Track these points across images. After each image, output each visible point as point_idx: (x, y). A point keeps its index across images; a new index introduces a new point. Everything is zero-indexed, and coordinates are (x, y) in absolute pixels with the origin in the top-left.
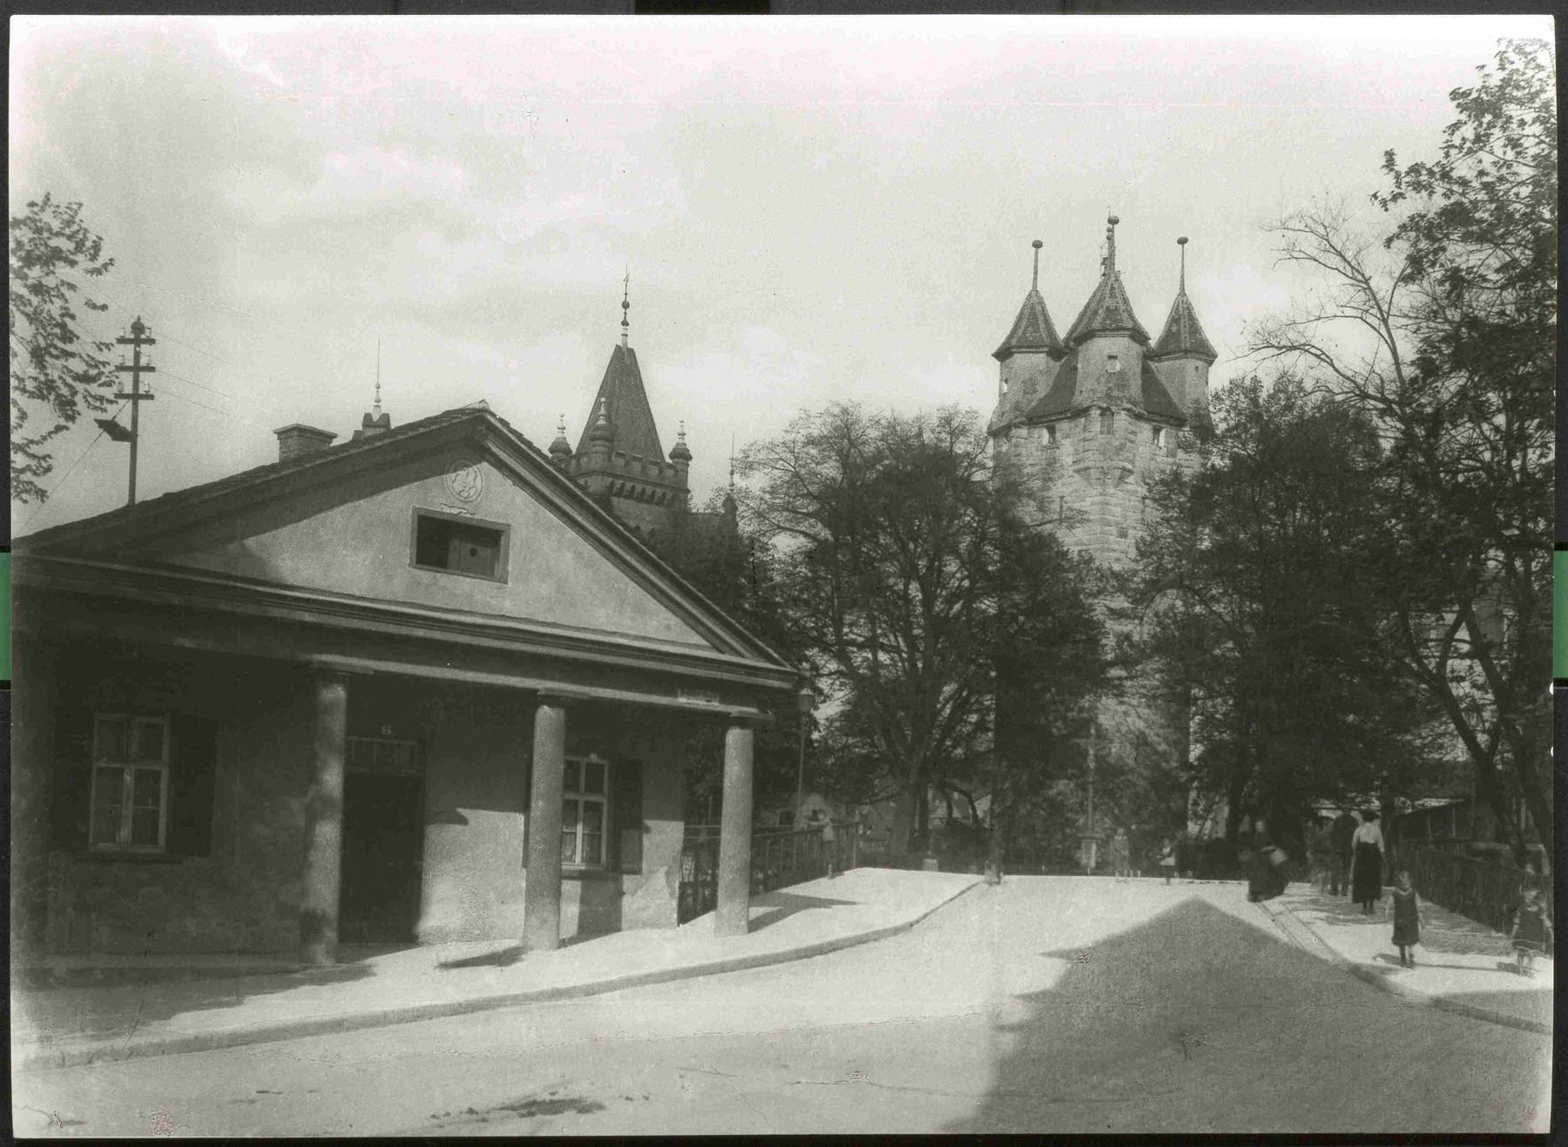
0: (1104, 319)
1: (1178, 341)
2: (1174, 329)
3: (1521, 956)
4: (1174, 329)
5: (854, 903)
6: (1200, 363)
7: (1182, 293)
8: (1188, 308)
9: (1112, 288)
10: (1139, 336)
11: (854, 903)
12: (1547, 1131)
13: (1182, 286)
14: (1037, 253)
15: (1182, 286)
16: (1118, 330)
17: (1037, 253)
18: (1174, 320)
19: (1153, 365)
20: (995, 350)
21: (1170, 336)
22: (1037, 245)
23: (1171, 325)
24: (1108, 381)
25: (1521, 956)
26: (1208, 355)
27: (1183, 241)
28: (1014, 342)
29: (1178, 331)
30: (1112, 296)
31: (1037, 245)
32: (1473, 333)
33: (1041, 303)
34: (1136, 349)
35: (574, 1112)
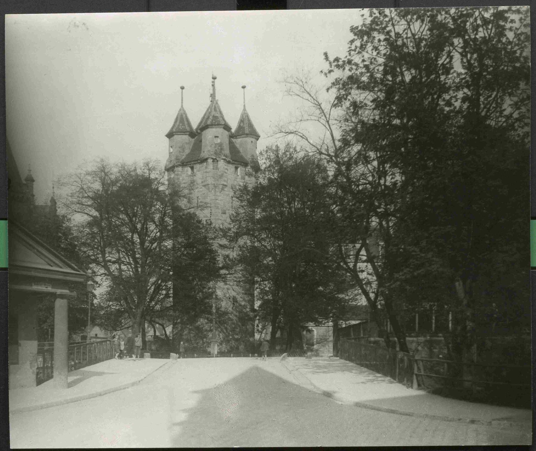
0: (212, 120)
2: (242, 124)
6: (253, 140)
8: (247, 116)
9: (215, 107)
10: (227, 128)
18: (242, 121)
22: (182, 88)
23: (240, 123)
27: (244, 87)
31: (182, 88)
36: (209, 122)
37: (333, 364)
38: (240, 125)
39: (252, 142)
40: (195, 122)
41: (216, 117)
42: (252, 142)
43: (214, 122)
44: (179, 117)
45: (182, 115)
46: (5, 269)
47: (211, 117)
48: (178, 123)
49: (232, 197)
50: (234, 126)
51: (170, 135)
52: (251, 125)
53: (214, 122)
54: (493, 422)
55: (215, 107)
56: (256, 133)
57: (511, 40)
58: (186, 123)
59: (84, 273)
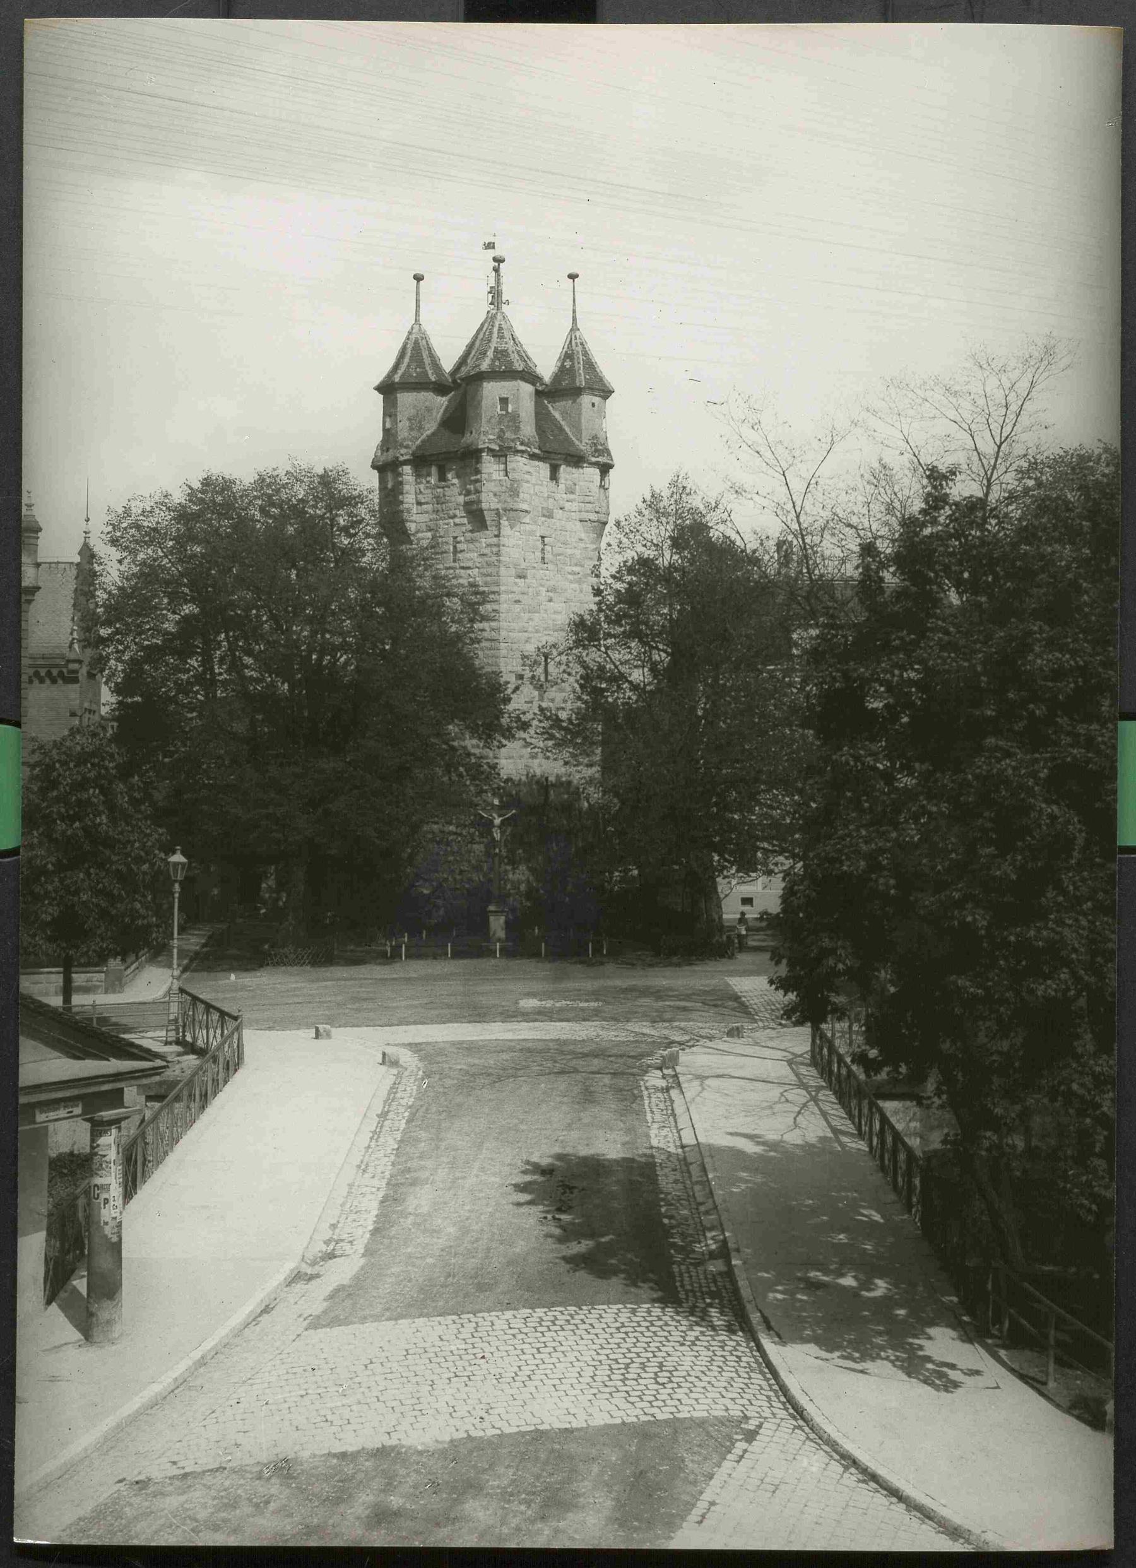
0: (493, 361)
1: (573, 378)
2: (568, 364)
3: (117, 684)
4: (568, 364)
5: (731, 1134)
6: (596, 400)
7: (574, 328)
8: (582, 344)
9: (500, 328)
10: (529, 376)
11: (731, 1134)
12: (1112, 1547)
13: (574, 319)
14: (418, 288)
15: (574, 319)
16: (510, 374)
17: (418, 288)
18: (568, 356)
19: (556, 412)
20: (377, 383)
21: (565, 372)
22: (418, 278)
23: (564, 361)
24: (500, 423)
25: (117, 684)
26: (603, 391)
27: (573, 277)
28: (397, 378)
29: (572, 366)
30: (501, 337)
31: (418, 278)
32: (948, 511)
33: (425, 338)
34: (527, 389)
35: (346, 1282)
36: (485, 366)
37: (764, 941)
38: (563, 366)
39: (593, 405)
40: (448, 359)
41: (502, 351)
42: (593, 405)
43: (497, 363)
44: (410, 347)
45: (416, 342)
46: (14, 852)
47: (490, 354)
48: (406, 360)
49: (543, 537)
50: (546, 368)
51: (387, 389)
52: (590, 366)
53: (497, 363)
54: (800, 1119)
55: (500, 328)
56: (604, 385)
57: (842, 555)
58: (427, 361)
59: (164, 1064)
